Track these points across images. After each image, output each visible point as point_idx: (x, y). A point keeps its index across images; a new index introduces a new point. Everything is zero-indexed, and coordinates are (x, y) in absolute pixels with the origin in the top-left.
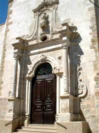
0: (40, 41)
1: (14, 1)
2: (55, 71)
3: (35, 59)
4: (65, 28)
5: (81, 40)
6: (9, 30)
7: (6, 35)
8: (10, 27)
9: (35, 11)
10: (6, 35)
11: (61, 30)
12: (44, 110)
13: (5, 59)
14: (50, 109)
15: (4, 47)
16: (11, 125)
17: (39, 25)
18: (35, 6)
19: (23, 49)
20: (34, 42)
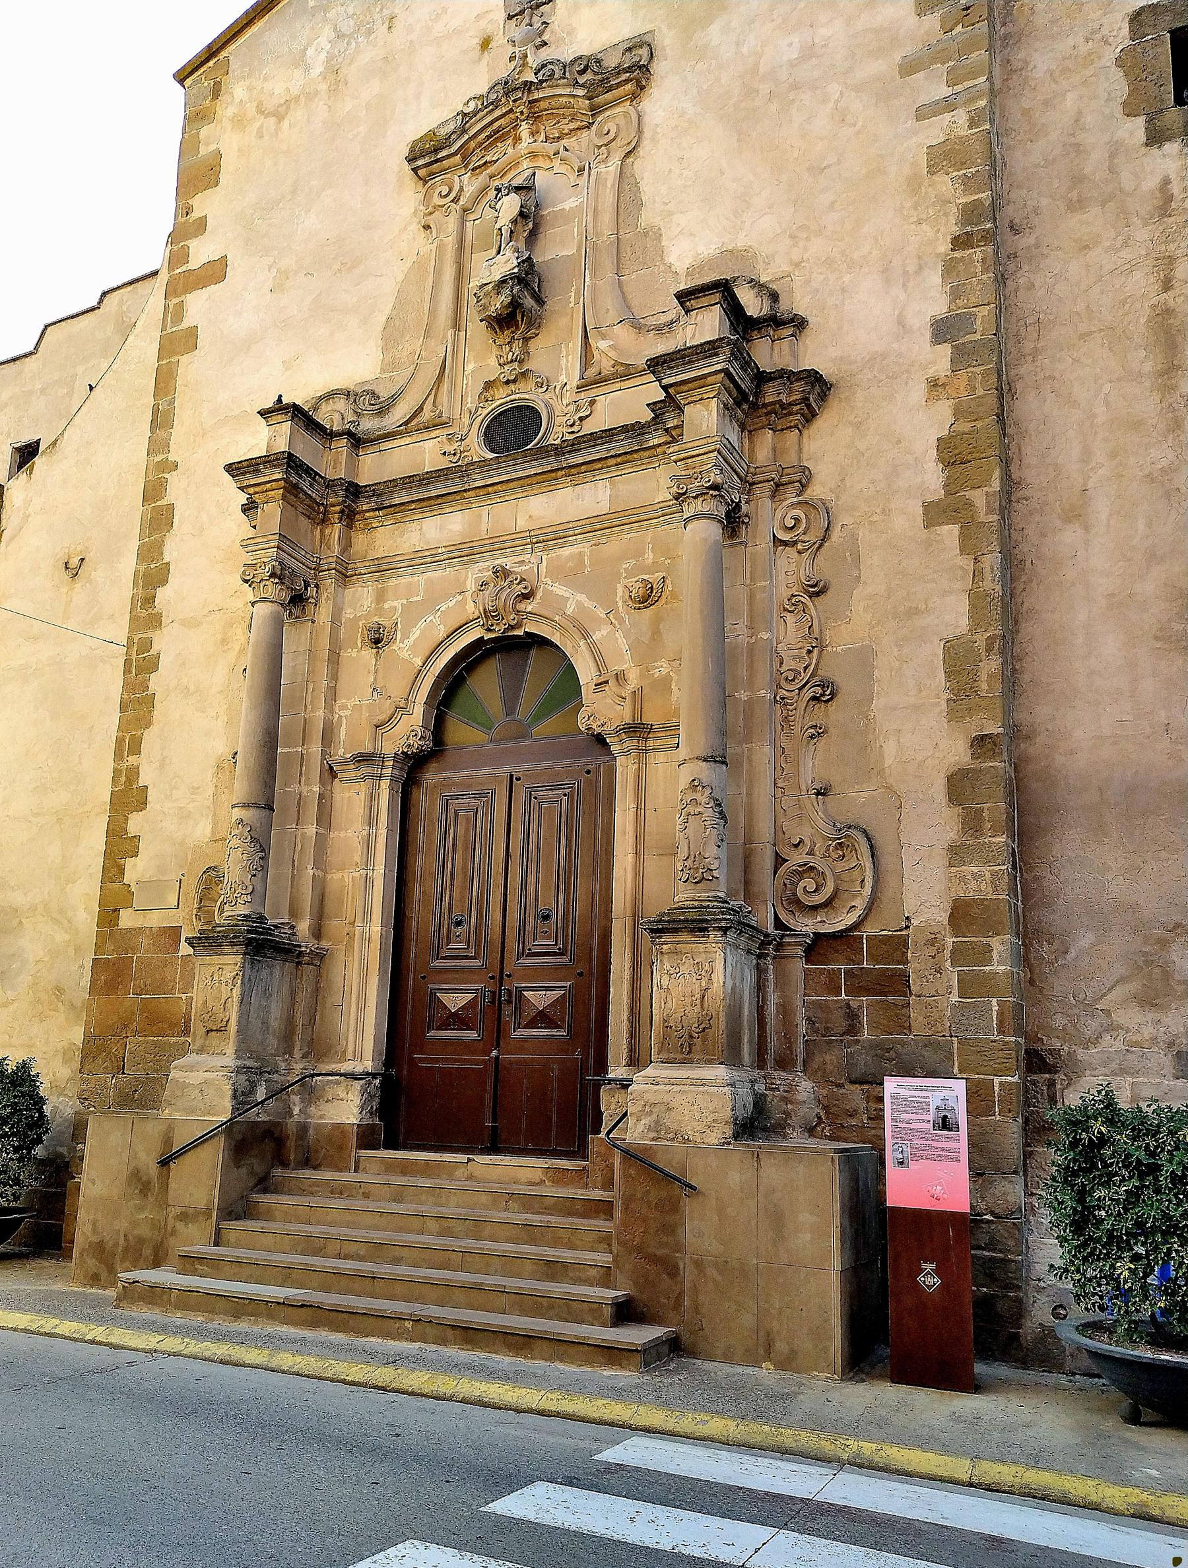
0: (478, 451)
1: (1159, 1457)
2: (601, 710)
3: (421, 593)
4: (708, 324)
5: (1120, 62)
6: (193, 332)
7: (165, 382)
8: (198, 306)
9: (428, 157)
10: (165, 382)
11: (662, 347)
12: (497, 1035)
13: (162, 594)
14: (550, 1023)
15: (154, 491)
16: (220, 1142)
17: (469, 301)
18: (432, 110)
19: (318, 486)
20: (427, 453)
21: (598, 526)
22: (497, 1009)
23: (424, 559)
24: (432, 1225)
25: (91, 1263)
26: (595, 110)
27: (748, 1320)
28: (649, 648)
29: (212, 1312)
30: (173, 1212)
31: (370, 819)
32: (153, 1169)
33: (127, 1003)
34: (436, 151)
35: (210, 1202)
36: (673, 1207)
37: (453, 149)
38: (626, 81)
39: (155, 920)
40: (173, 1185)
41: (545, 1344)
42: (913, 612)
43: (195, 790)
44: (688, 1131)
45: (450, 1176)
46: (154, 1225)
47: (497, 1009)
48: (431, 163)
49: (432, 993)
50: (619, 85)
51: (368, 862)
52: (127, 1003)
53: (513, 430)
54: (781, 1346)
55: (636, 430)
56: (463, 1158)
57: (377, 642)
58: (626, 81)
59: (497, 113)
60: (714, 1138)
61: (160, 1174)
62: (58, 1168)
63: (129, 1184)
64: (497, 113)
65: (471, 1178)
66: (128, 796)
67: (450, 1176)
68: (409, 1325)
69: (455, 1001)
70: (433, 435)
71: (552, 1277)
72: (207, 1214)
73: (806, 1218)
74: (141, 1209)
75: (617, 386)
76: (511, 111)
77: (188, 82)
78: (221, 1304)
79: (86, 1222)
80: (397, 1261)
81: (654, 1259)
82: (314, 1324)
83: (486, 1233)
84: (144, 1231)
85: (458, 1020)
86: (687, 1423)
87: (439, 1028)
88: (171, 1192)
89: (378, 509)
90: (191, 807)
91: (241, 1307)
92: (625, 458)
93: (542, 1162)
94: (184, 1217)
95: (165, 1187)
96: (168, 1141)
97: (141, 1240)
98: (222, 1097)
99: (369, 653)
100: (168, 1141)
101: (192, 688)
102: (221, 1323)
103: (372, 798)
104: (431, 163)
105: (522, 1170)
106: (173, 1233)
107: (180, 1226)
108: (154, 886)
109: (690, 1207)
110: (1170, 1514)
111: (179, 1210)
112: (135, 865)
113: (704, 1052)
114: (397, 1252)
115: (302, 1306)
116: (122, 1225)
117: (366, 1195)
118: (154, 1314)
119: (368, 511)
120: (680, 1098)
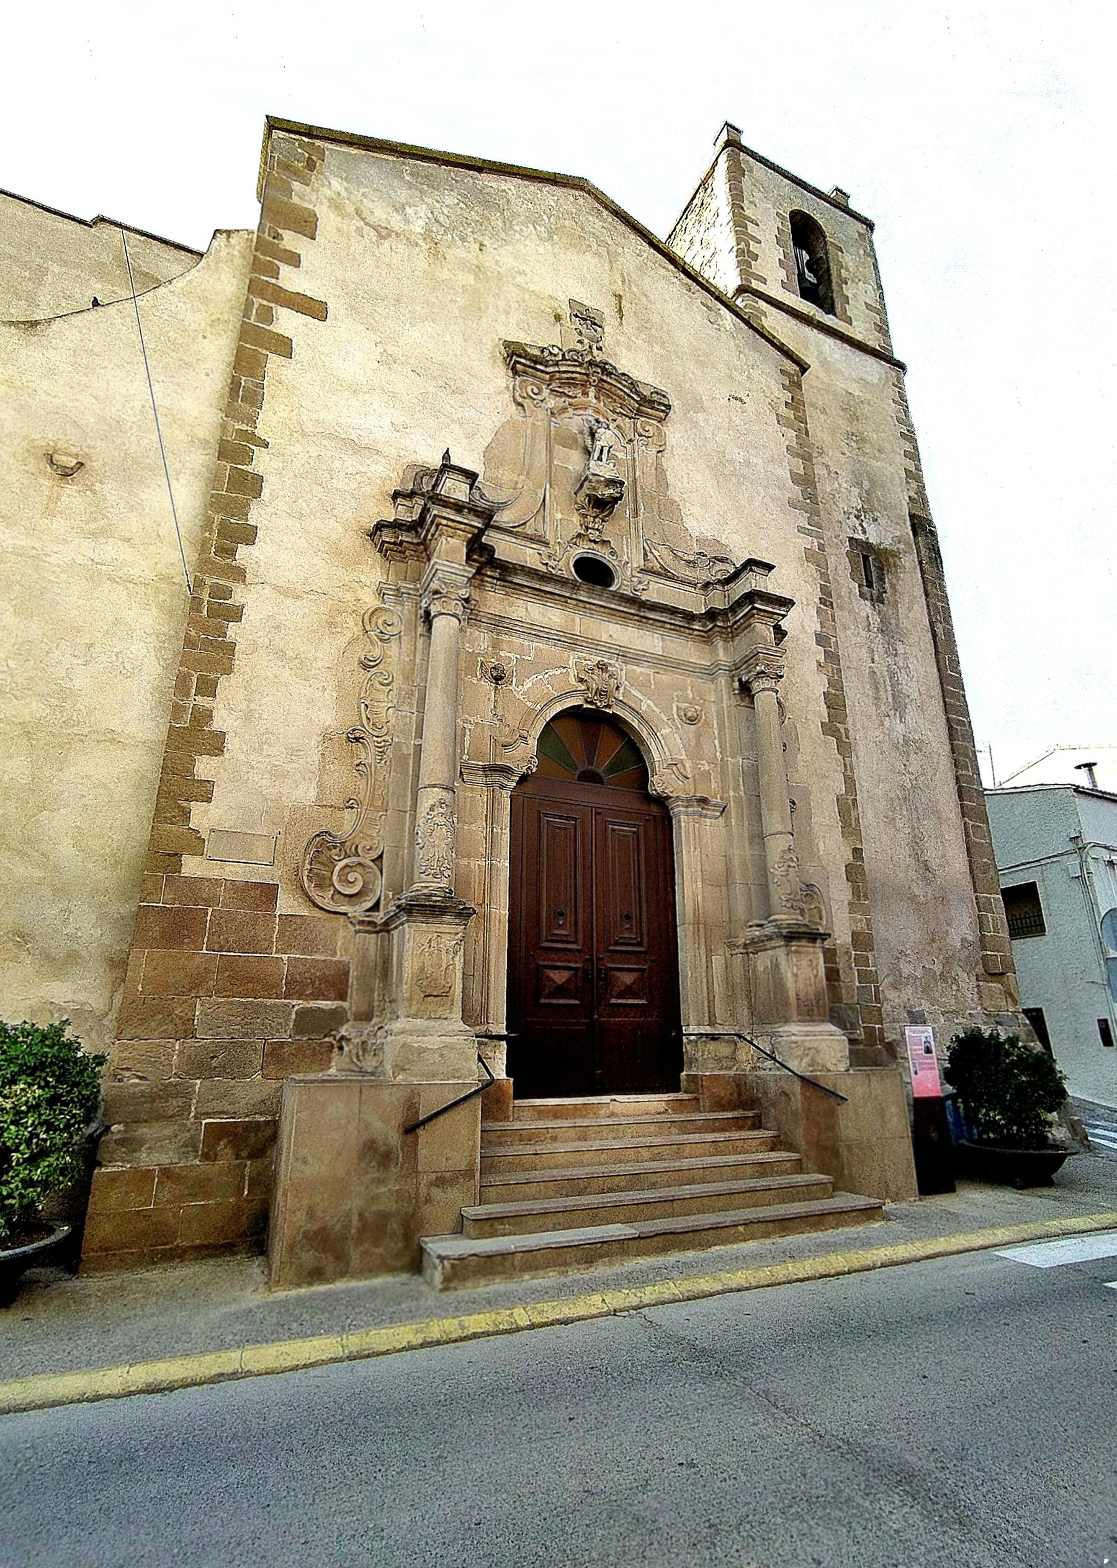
16: (478, 1101)
21: (662, 663)
22: (591, 983)
23: (536, 632)
24: (645, 1154)
25: (308, 1257)
26: (639, 413)
27: (876, 1175)
28: (696, 750)
29: (565, 1264)
30: (424, 1180)
31: (492, 818)
32: (394, 1138)
33: (198, 960)
34: (536, 362)
35: (472, 1163)
36: (831, 1113)
37: (547, 370)
38: (663, 411)
39: (235, 872)
40: (423, 1152)
41: (831, 1217)
42: (824, 777)
43: (293, 753)
44: (829, 1065)
45: (596, 1115)
46: (399, 1195)
47: (591, 983)
48: (529, 367)
49: (539, 969)
50: (658, 410)
51: (491, 853)
52: (198, 960)
53: (595, 573)
54: (893, 1187)
55: (689, 617)
56: (606, 1099)
57: (498, 679)
58: (663, 411)
59: (578, 369)
60: (842, 1067)
61: (404, 1143)
62: (370, 1148)
63: (361, 1157)
64: (578, 369)
65: (612, 1115)
66: (189, 738)
67: (596, 1115)
68: (741, 1229)
69: (560, 977)
70: (534, 546)
71: (763, 1175)
72: (469, 1173)
73: (893, 1109)
74: (380, 1182)
75: (663, 581)
76: (587, 375)
77: (277, 134)
78: (570, 1255)
79: (290, 1218)
80: (653, 1186)
81: (825, 1148)
82: (664, 1250)
83: (686, 1154)
84: (388, 1205)
85: (561, 991)
86: (1054, 1225)
87: (617, 997)
88: (421, 1158)
89: (498, 579)
90: (289, 767)
91: (591, 1253)
92: (676, 628)
93: (665, 1097)
94: (441, 1182)
95: (412, 1154)
96: (411, 1106)
97: (383, 1217)
98: (467, 1060)
99: (487, 686)
100: (411, 1106)
101: (290, 653)
102: (577, 1274)
103: (493, 801)
104: (529, 367)
105: (653, 1102)
106: (428, 1200)
107: (435, 1192)
108: (236, 838)
109: (840, 1110)
110: (255, 1367)
111: (433, 1177)
112: (206, 812)
113: (820, 1014)
114: (653, 1178)
115: (657, 1235)
116: (355, 1204)
117: (554, 1139)
118: (499, 1285)
119: (489, 576)
120: (823, 1044)
